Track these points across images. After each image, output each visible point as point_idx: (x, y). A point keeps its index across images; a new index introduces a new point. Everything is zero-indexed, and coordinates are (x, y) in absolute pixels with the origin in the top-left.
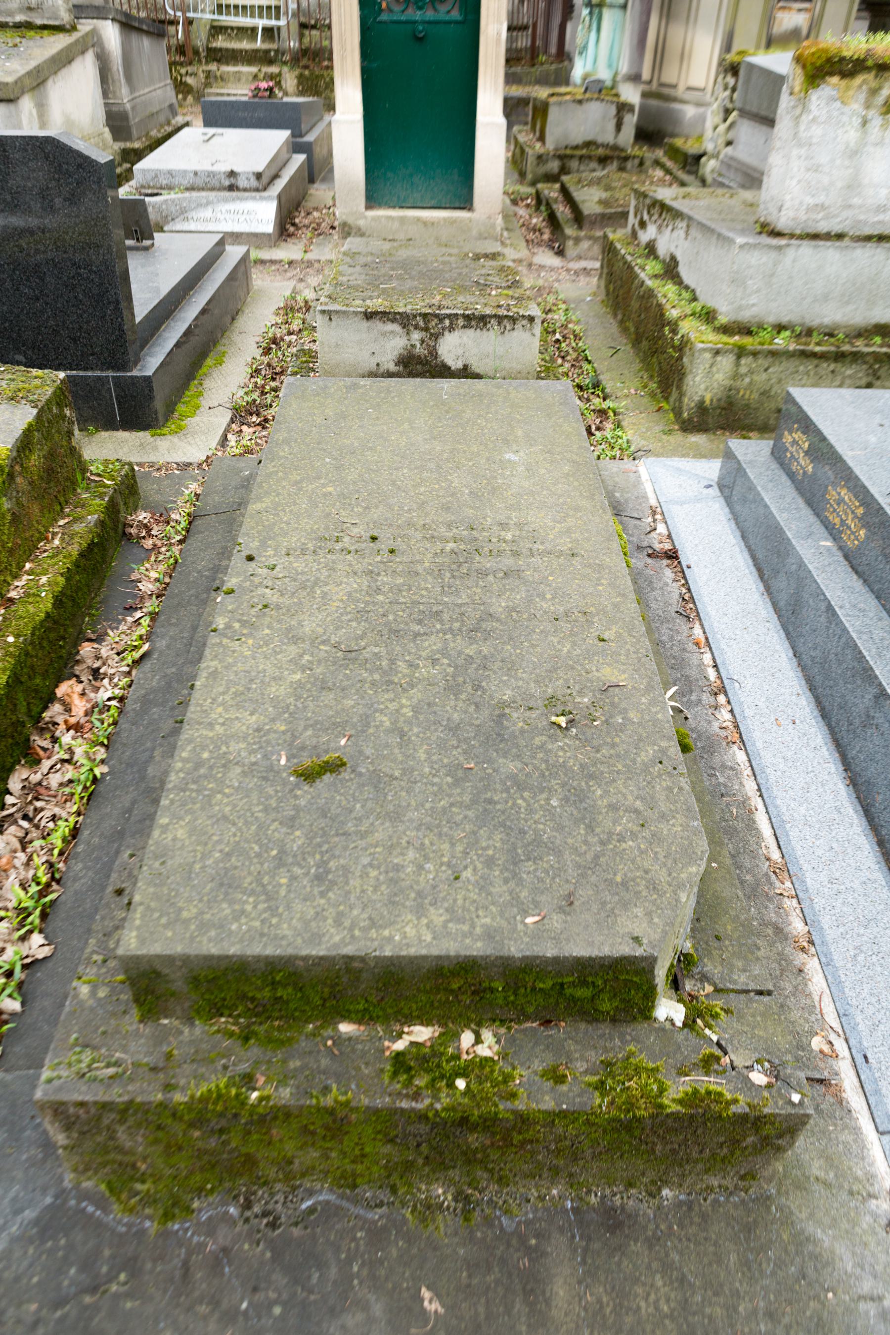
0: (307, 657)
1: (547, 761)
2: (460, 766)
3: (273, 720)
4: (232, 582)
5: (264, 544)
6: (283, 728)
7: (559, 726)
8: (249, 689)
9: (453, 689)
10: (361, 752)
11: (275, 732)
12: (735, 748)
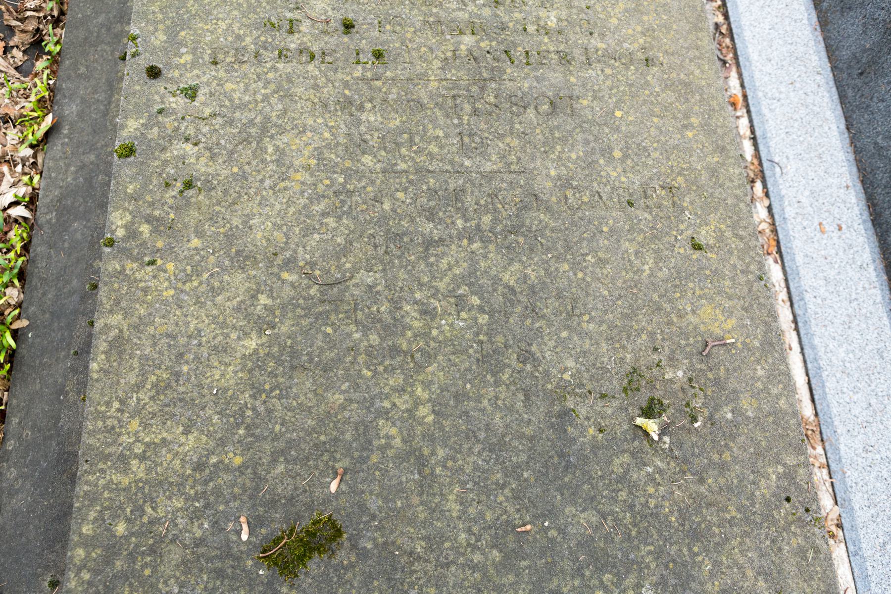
0: (263, 299)
1: (632, 507)
2: (510, 526)
3: (222, 443)
4: (131, 127)
5: (174, 43)
6: (238, 460)
7: (646, 434)
8: (178, 375)
9: (490, 362)
10: (362, 507)
11: (227, 469)
12: (770, 260)
